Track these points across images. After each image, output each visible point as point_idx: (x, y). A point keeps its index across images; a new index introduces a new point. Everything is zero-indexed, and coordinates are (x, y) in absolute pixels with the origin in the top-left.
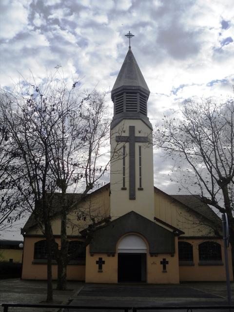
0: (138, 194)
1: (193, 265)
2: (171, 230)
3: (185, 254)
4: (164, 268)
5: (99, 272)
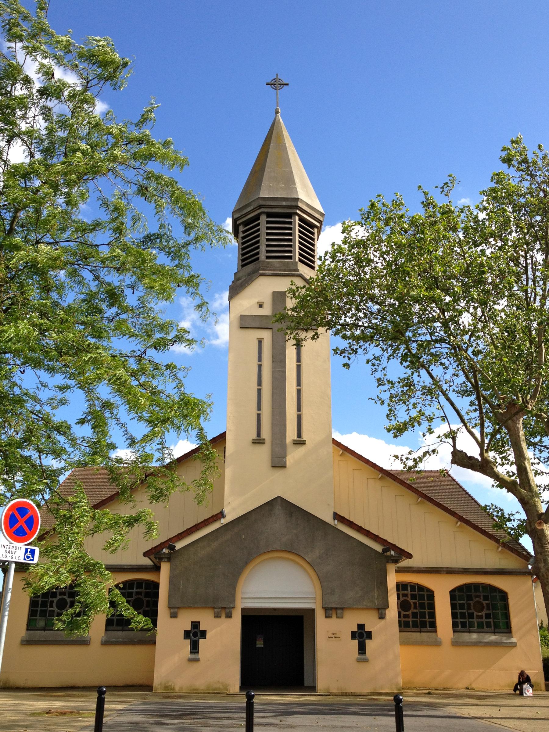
0: (293, 456)
1: (437, 643)
2: (378, 548)
3: (417, 612)
4: (362, 649)
5: (358, 660)
